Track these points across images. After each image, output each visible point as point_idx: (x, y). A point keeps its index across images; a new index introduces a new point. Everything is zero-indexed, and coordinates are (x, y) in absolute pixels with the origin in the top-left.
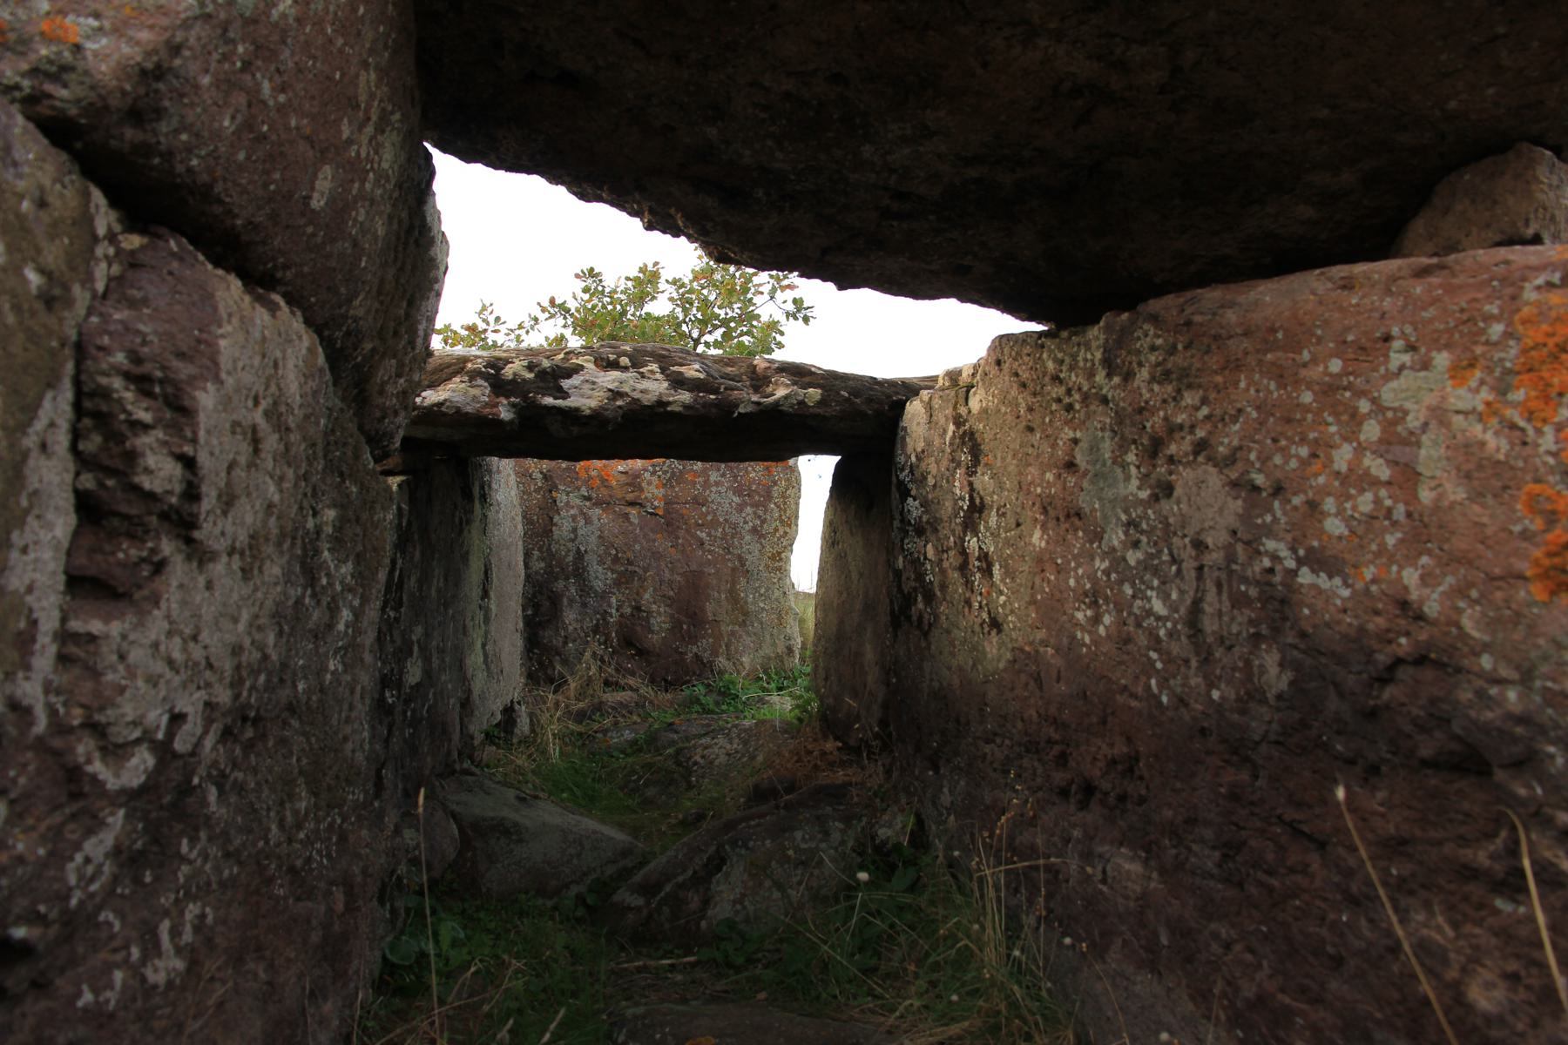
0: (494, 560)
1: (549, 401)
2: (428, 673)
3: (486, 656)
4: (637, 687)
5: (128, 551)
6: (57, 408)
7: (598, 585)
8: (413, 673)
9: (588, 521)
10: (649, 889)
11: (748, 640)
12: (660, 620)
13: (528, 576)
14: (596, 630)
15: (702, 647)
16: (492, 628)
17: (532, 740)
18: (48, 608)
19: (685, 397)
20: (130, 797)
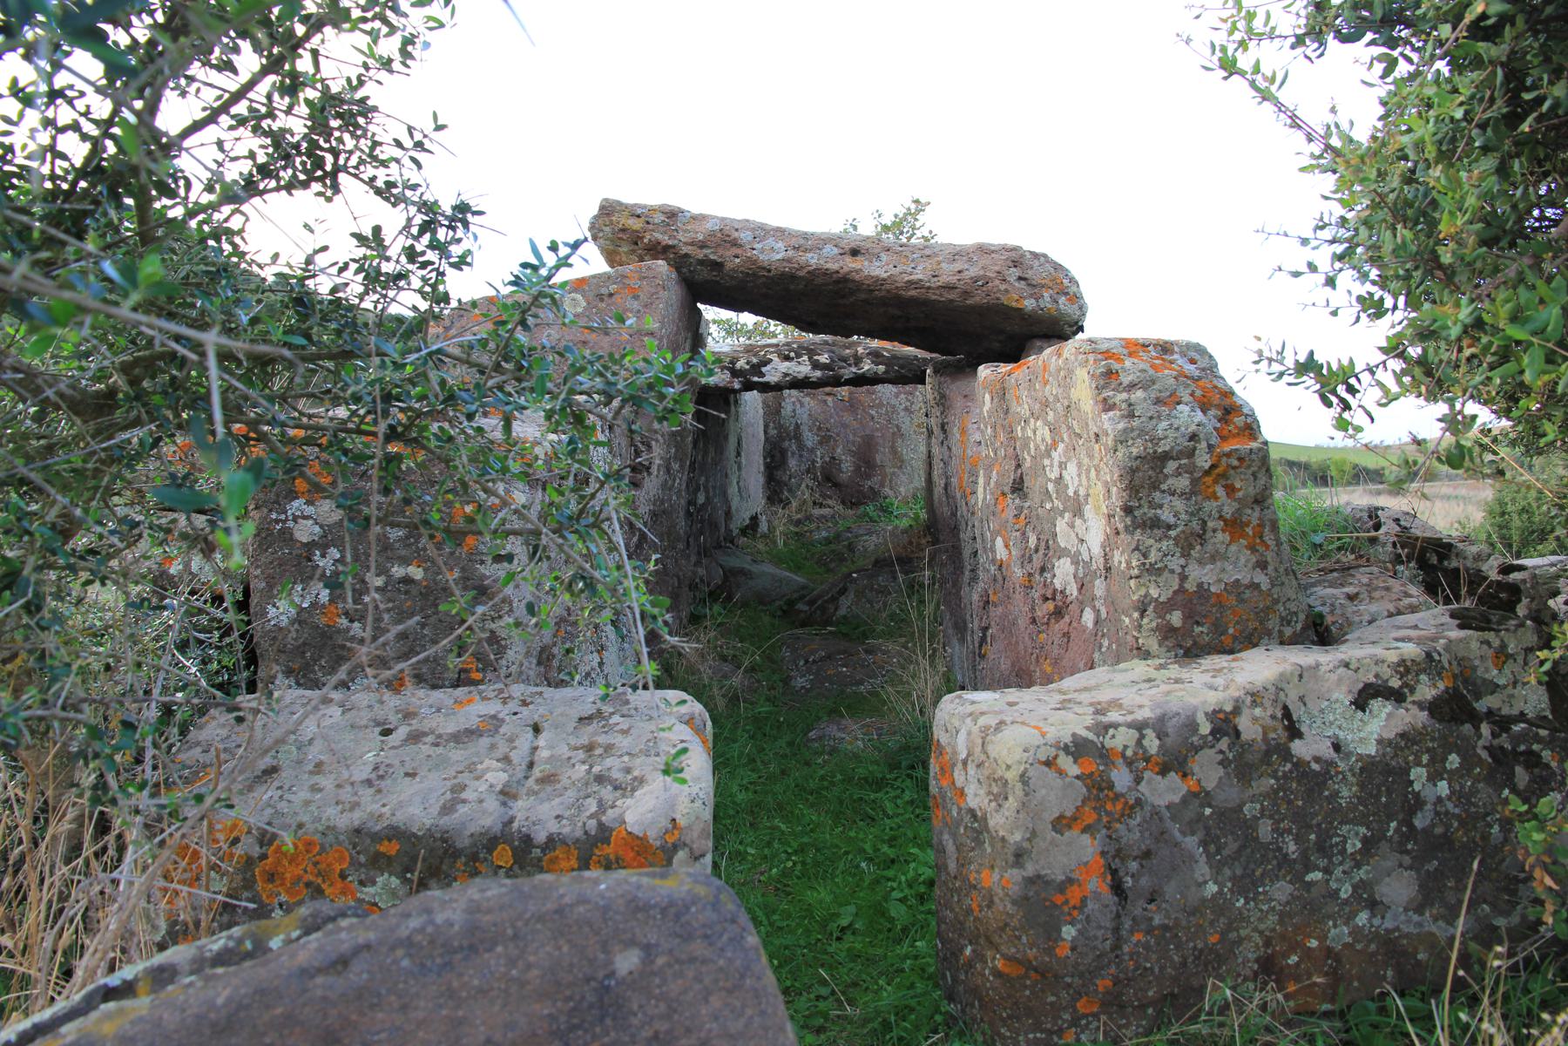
1: (756, 379)
2: (707, 498)
4: (834, 506)
7: (809, 444)
8: (701, 499)
9: (802, 405)
10: (811, 603)
11: (904, 478)
12: (847, 465)
13: (767, 439)
14: (808, 471)
15: (874, 482)
16: (743, 472)
17: (769, 537)
19: (818, 373)
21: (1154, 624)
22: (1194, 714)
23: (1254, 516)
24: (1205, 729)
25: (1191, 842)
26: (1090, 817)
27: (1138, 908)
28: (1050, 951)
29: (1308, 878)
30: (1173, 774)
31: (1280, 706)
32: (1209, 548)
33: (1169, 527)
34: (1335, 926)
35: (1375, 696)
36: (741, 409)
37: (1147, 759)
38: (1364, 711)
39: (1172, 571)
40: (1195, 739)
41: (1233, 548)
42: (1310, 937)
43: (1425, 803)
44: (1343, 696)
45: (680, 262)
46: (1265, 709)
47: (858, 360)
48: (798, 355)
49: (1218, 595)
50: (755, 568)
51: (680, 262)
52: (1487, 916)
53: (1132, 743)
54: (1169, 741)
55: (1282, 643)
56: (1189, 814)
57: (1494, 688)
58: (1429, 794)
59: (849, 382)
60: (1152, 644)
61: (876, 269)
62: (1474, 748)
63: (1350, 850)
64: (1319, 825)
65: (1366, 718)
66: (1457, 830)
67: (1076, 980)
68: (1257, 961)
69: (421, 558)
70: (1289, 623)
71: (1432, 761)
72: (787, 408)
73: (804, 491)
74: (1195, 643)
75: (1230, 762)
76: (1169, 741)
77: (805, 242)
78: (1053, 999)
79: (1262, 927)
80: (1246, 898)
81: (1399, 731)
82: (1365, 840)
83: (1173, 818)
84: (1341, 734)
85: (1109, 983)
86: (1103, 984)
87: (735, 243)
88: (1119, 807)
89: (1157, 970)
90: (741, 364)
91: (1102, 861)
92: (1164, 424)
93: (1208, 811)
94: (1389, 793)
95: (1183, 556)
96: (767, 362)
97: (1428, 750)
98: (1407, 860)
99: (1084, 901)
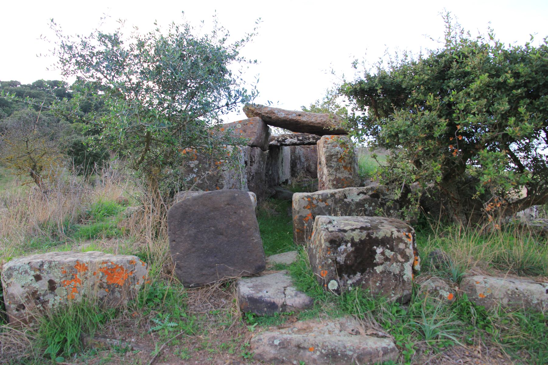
7: (303, 161)
8: (270, 172)
17: (291, 185)
19: (299, 142)
23: (349, 166)
24: (329, 196)
26: (309, 207)
36: (283, 151)
44: (356, 193)
45: (262, 117)
47: (309, 138)
50: (284, 191)
51: (262, 117)
57: (387, 195)
58: (368, 209)
59: (306, 144)
60: (331, 187)
61: (304, 119)
72: (297, 151)
73: (301, 174)
77: (289, 113)
87: (274, 113)
90: (280, 139)
96: (286, 139)
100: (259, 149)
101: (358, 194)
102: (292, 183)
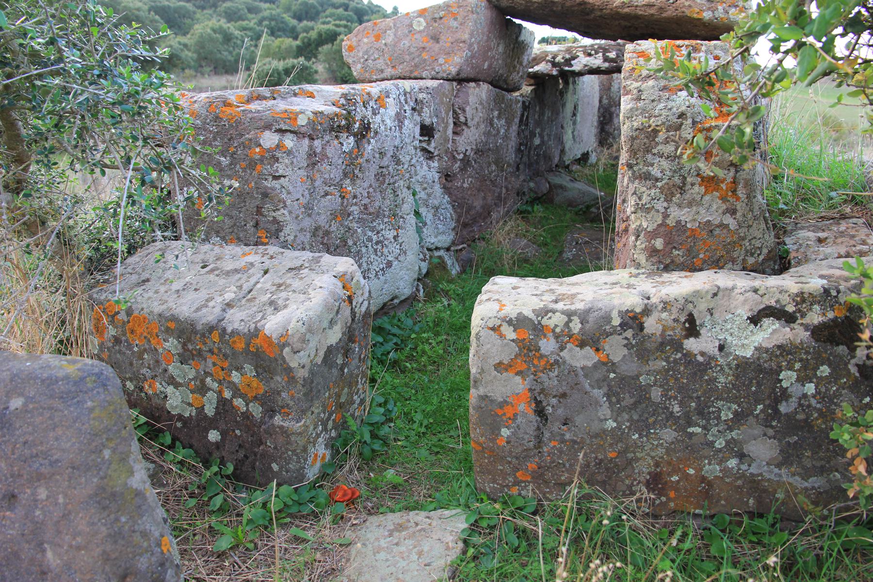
0: (579, 103)
1: (567, 68)
2: (543, 142)
3: (573, 136)
5: (459, 129)
6: (451, 113)
16: (578, 127)
18: (451, 136)
19: (607, 65)
20: (461, 160)
21: (643, 246)
22: (611, 311)
24: (616, 321)
25: (598, 393)
27: (556, 427)
28: (493, 440)
29: (690, 430)
30: (588, 348)
31: (686, 313)
32: (687, 196)
33: (657, 180)
34: (710, 464)
35: (768, 316)
36: (579, 87)
37: (570, 337)
38: (756, 325)
39: (658, 211)
40: (607, 327)
41: (707, 198)
42: (689, 467)
43: (790, 396)
44: (744, 313)
46: (670, 314)
48: (597, 53)
49: (692, 230)
50: (570, 185)
52: (837, 480)
53: (561, 324)
54: (588, 326)
55: (744, 269)
56: (597, 375)
58: (796, 390)
60: (642, 259)
62: (846, 364)
63: (723, 418)
64: (698, 398)
65: (755, 331)
66: (817, 419)
67: (514, 460)
68: (649, 473)
69: (238, 178)
70: (752, 255)
71: (805, 368)
74: (673, 261)
75: (633, 346)
76: (588, 326)
78: (501, 468)
79: (653, 454)
80: (640, 435)
81: (778, 343)
82: (736, 413)
83: (586, 376)
84: (729, 339)
85: (534, 466)
86: (532, 465)
88: (542, 363)
89: (567, 465)
90: (559, 59)
91: (529, 394)
92: (661, 106)
93: (612, 375)
94: (759, 385)
95: (666, 200)
96: (574, 58)
97: (801, 360)
98: (771, 432)
99: (515, 415)
100: (485, 87)
101: (755, 320)
102: (598, 160)
